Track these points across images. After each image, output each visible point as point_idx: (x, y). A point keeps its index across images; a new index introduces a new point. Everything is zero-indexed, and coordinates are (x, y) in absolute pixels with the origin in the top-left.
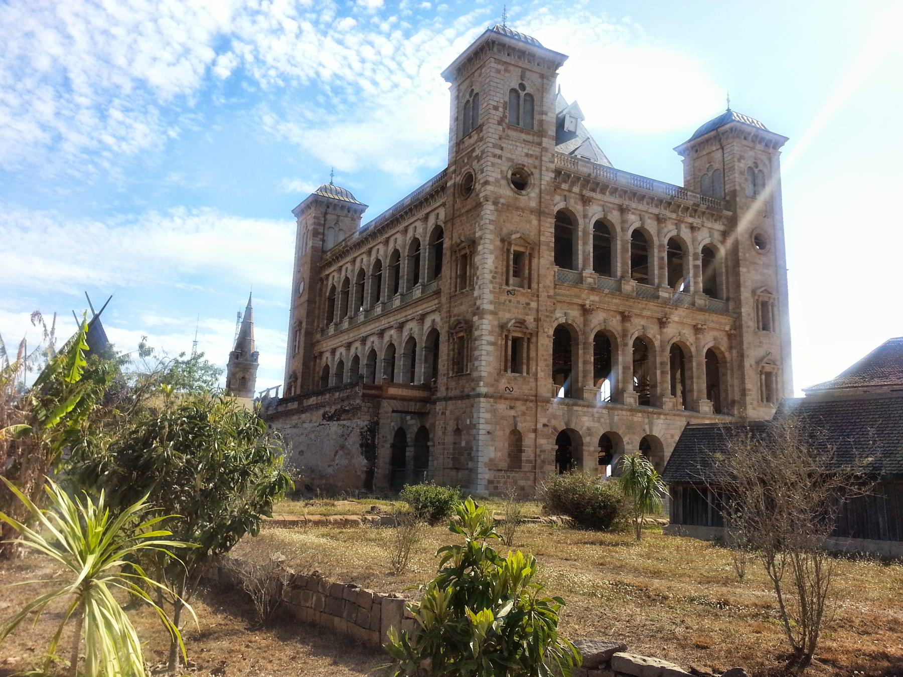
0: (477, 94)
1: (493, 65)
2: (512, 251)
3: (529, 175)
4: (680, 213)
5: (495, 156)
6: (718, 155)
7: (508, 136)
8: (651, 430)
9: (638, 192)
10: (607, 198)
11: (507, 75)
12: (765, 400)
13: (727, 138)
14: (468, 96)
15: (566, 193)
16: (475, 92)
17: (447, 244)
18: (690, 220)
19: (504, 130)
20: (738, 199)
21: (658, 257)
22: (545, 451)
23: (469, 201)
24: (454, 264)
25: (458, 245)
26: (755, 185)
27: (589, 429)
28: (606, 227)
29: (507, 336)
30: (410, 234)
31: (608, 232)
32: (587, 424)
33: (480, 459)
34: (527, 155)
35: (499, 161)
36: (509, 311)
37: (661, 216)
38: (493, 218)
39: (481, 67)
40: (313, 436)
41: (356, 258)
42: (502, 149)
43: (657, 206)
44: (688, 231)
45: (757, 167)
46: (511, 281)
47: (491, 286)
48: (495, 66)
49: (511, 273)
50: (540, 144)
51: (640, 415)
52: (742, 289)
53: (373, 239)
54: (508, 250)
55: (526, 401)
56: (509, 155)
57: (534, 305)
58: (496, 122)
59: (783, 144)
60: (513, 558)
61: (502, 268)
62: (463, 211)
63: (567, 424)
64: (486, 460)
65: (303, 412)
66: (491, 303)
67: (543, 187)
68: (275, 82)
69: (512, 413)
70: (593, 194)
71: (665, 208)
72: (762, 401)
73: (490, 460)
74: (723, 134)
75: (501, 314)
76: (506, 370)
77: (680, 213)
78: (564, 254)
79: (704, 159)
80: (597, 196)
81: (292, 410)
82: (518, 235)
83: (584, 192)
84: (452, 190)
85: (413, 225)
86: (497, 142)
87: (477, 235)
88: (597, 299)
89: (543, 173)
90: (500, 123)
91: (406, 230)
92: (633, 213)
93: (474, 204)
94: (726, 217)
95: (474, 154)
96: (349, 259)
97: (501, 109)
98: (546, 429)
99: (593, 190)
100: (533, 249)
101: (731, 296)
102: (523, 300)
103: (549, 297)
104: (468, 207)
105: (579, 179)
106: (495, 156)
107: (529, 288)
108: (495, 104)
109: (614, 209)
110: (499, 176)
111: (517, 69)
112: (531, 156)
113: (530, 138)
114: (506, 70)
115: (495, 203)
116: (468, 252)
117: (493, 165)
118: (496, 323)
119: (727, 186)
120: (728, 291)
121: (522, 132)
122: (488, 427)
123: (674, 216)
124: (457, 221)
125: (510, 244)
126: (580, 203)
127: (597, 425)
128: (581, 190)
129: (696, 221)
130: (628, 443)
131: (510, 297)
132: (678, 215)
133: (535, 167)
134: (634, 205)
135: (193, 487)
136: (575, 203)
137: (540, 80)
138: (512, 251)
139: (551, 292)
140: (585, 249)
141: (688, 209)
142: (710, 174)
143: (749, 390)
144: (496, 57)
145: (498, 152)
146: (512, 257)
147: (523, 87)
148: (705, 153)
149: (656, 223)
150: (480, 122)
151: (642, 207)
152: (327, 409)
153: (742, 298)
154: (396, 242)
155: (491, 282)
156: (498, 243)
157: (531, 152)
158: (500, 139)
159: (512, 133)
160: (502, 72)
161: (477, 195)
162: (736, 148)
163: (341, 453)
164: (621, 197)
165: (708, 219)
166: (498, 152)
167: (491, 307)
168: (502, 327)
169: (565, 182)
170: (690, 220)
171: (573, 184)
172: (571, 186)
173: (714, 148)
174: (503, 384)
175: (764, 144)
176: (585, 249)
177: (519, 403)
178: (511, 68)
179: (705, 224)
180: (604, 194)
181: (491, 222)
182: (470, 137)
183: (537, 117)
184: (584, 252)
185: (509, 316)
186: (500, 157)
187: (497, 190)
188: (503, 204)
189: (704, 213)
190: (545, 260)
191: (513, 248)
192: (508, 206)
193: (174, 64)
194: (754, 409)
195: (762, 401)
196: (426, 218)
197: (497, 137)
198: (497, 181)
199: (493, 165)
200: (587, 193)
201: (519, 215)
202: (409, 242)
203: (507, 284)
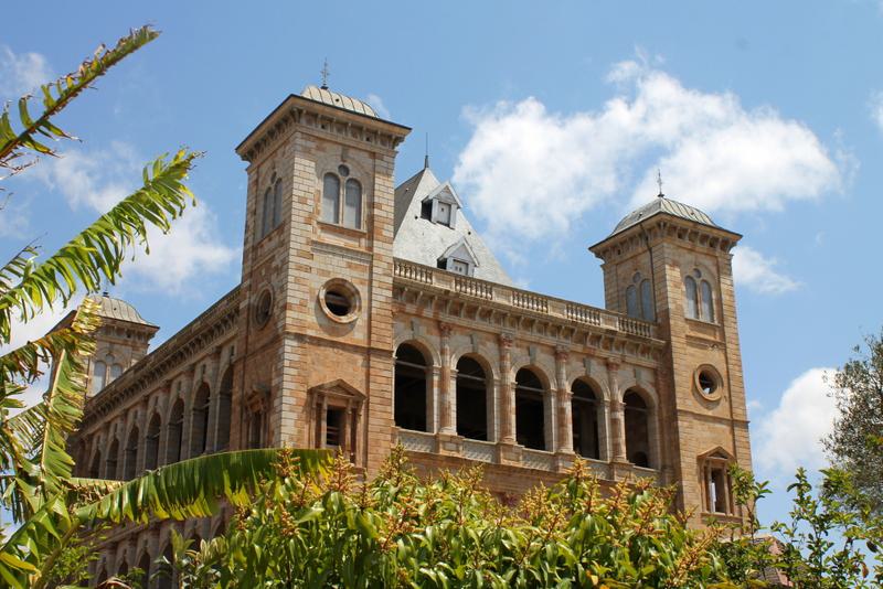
0: (280, 180)
1: (299, 141)
2: (325, 407)
3: (353, 295)
4: (589, 344)
6: (645, 259)
9: (526, 318)
13: (655, 235)
14: (269, 182)
15: (413, 319)
16: (278, 177)
17: (237, 395)
18: (605, 354)
20: (672, 322)
21: (560, 411)
23: (266, 331)
24: (245, 426)
25: (250, 398)
30: (198, 377)
35: (306, 275)
37: (560, 349)
39: (285, 143)
41: (128, 410)
43: (553, 334)
44: (603, 369)
48: (303, 142)
49: (324, 439)
53: (150, 382)
54: (319, 406)
58: (302, 220)
59: (734, 244)
60: (848, 404)
62: (258, 346)
71: (566, 337)
74: (650, 230)
77: (589, 344)
78: (411, 409)
79: (629, 265)
84: (245, 315)
85: (201, 364)
87: (274, 383)
89: (374, 290)
91: (192, 370)
93: (271, 336)
95: (274, 264)
96: (118, 411)
99: (456, 313)
100: (358, 403)
101: (668, 462)
104: (265, 341)
105: (432, 298)
111: (335, 147)
114: (318, 148)
116: (262, 407)
119: (658, 304)
120: (664, 458)
123: (579, 348)
124: (250, 361)
125: (322, 396)
126: (435, 331)
129: (613, 355)
132: (585, 347)
135: (280, 544)
136: (428, 332)
137: (371, 161)
138: (325, 407)
140: (444, 397)
141: (599, 338)
142: (637, 285)
144: (304, 130)
146: (325, 415)
148: (629, 256)
149: (553, 358)
150: (282, 219)
151: (533, 335)
153: (683, 465)
154: (179, 389)
160: (313, 151)
161: (275, 324)
162: (667, 251)
164: (498, 321)
165: (631, 351)
169: (411, 302)
170: (605, 354)
172: (420, 309)
173: (640, 250)
176: (444, 397)
178: (325, 145)
180: (472, 318)
182: (270, 240)
187: (301, 316)
189: (623, 343)
190: (381, 413)
196: (218, 353)
198: (303, 305)
200: (446, 318)
202: (196, 387)
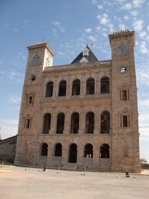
0: (39, 57)
8: (72, 141)
10: (64, 73)
19: (30, 68)
22: (33, 149)
27: (50, 142)
32: (49, 141)
33: (16, 151)
34: (36, 71)
40: (8, 148)
46: (28, 105)
51: (69, 137)
55: (29, 136)
57: (33, 109)
63: (43, 141)
64: (18, 151)
68: (135, 23)
69: (26, 139)
70: (58, 74)
73: (19, 151)
76: (24, 128)
80: (60, 74)
82: (29, 93)
88: (56, 104)
92: (73, 75)
98: (34, 143)
107: (33, 105)
109: (66, 76)
110: (27, 79)
112: (37, 71)
114: (32, 54)
118: (22, 116)
122: (19, 143)
123: (88, 71)
127: (53, 141)
130: (64, 146)
133: (37, 74)
134: (72, 73)
147: (37, 55)
152: (11, 142)
157: (37, 70)
163: (13, 152)
174: (24, 131)
175: (118, 37)
177: (27, 137)
178: (34, 53)
179: (101, 70)
191: (29, 96)
194: (116, 130)
200: (56, 74)
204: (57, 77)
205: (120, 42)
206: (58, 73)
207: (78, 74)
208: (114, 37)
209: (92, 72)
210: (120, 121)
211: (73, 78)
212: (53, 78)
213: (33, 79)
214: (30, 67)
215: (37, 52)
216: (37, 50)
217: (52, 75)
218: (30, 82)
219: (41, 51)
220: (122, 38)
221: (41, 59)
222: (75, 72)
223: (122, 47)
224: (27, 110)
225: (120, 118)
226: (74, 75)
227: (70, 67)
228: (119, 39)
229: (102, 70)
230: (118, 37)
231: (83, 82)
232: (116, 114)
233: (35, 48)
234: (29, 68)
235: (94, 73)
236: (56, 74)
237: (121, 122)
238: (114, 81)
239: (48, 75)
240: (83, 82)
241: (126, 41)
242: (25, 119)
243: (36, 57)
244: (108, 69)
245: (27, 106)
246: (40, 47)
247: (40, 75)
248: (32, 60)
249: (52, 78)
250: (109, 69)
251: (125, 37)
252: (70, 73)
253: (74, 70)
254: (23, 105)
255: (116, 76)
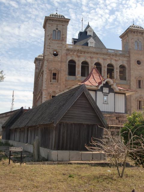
2: (52, 73)
5: (48, 48)
7: (52, 42)
10: (86, 55)
11: (52, 27)
12: (138, 109)
18: (115, 58)
19: (51, 41)
26: (138, 46)
28: (87, 63)
29: (50, 96)
31: (139, 62)
34: (58, 47)
35: (49, 49)
36: (51, 89)
38: (46, 65)
42: (50, 46)
45: (139, 40)
46: (52, 81)
47: (45, 83)
49: (52, 78)
50: (62, 43)
52: (131, 77)
56: (52, 48)
57: (59, 87)
61: (49, 77)
65: (7, 117)
66: (46, 87)
67: (62, 55)
70: (81, 55)
72: (138, 109)
75: (49, 90)
80: (83, 55)
81: (4, 116)
82: (54, 68)
83: (78, 54)
86: (49, 45)
90: (49, 40)
92: (95, 58)
94: (127, 56)
97: (50, 36)
102: (55, 85)
103: (64, 84)
106: (48, 48)
107: (58, 82)
108: (48, 35)
109: (88, 58)
110: (49, 53)
112: (59, 47)
113: (59, 42)
114: (52, 26)
115: (47, 61)
117: (47, 51)
118: (47, 92)
121: (56, 41)
123: (109, 58)
125: (51, 71)
128: (77, 54)
131: (52, 85)
133: (60, 50)
137: (62, 27)
139: (64, 83)
143: (133, 106)
145: (49, 47)
147: (57, 29)
155: (46, 82)
156: (48, 71)
157: (59, 46)
158: (49, 44)
159: (53, 42)
166: (49, 47)
167: (46, 88)
168: (49, 93)
171: (74, 52)
175: (136, 33)
178: (54, 25)
179: (120, 59)
181: (46, 66)
183: (61, 36)
184: (78, 70)
185: (51, 91)
186: (49, 48)
188: (50, 61)
192: (51, 61)
193: (137, 6)
195: (138, 109)
197: (49, 43)
199: (47, 51)
200: (79, 54)
201: (55, 63)
203: (51, 82)
204: (79, 57)
205: (137, 37)
206: (80, 53)
207: (100, 58)
208: (133, 31)
209: (112, 59)
210: (137, 104)
211: (82, 59)
212: (76, 57)
213: (56, 55)
214: (51, 40)
215: (57, 25)
216: (58, 23)
217: (75, 54)
218: (52, 58)
219: (63, 25)
220: (139, 34)
221: (64, 35)
222: (97, 56)
223: (138, 42)
224: (52, 86)
225: (137, 102)
226: (96, 58)
227: (92, 49)
228: (136, 34)
229: (121, 58)
230: (136, 33)
231: (104, 67)
232: (134, 99)
233: (55, 20)
234: (50, 41)
235: (114, 60)
236: (79, 54)
237: (137, 105)
238: (132, 71)
239: (71, 53)
240: (117, 69)
241: (141, 37)
242: (50, 96)
243: (57, 31)
244: (125, 59)
245: (51, 82)
246: (52, 20)
247: (64, 52)
248: (52, 33)
249: (74, 57)
250: (127, 59)
251: (133, 32)
252: (92, 55)
253: (97, 54)
254: (47, 80)
255: (134, 67)
